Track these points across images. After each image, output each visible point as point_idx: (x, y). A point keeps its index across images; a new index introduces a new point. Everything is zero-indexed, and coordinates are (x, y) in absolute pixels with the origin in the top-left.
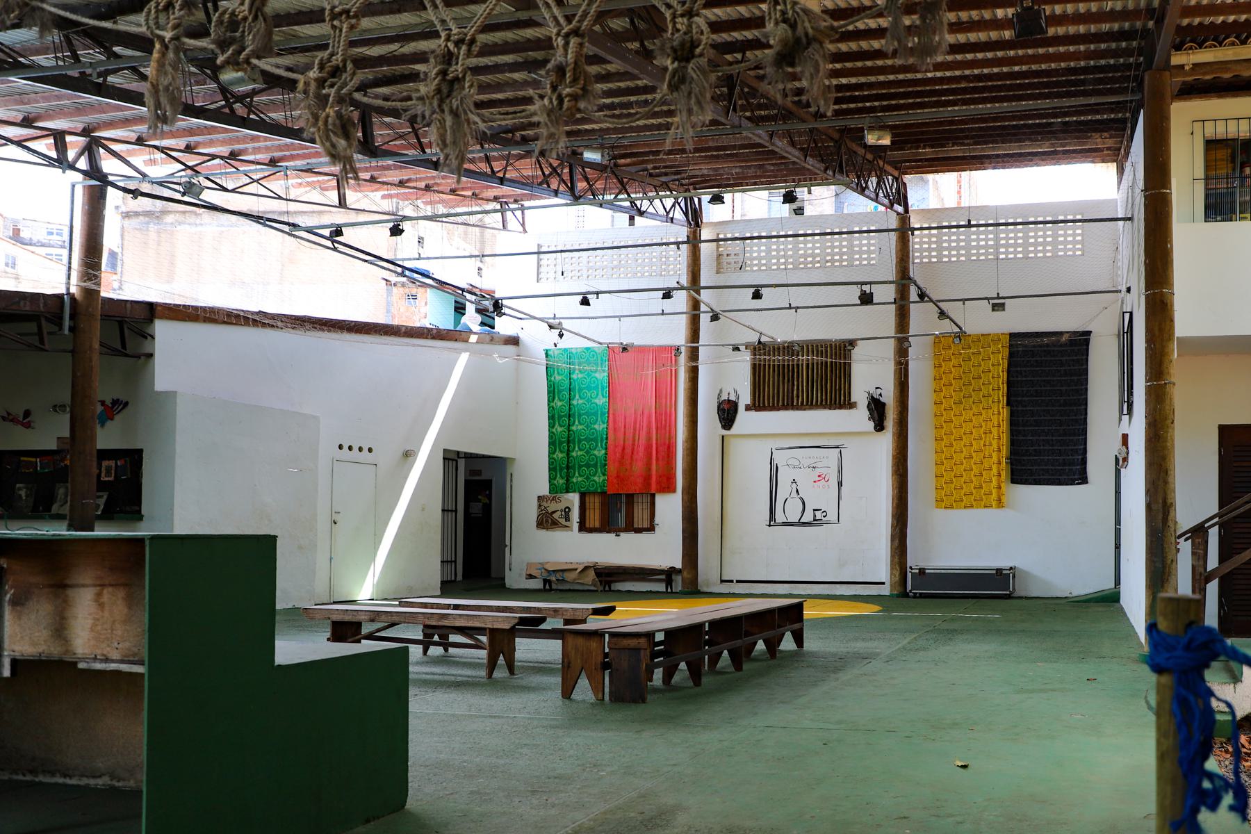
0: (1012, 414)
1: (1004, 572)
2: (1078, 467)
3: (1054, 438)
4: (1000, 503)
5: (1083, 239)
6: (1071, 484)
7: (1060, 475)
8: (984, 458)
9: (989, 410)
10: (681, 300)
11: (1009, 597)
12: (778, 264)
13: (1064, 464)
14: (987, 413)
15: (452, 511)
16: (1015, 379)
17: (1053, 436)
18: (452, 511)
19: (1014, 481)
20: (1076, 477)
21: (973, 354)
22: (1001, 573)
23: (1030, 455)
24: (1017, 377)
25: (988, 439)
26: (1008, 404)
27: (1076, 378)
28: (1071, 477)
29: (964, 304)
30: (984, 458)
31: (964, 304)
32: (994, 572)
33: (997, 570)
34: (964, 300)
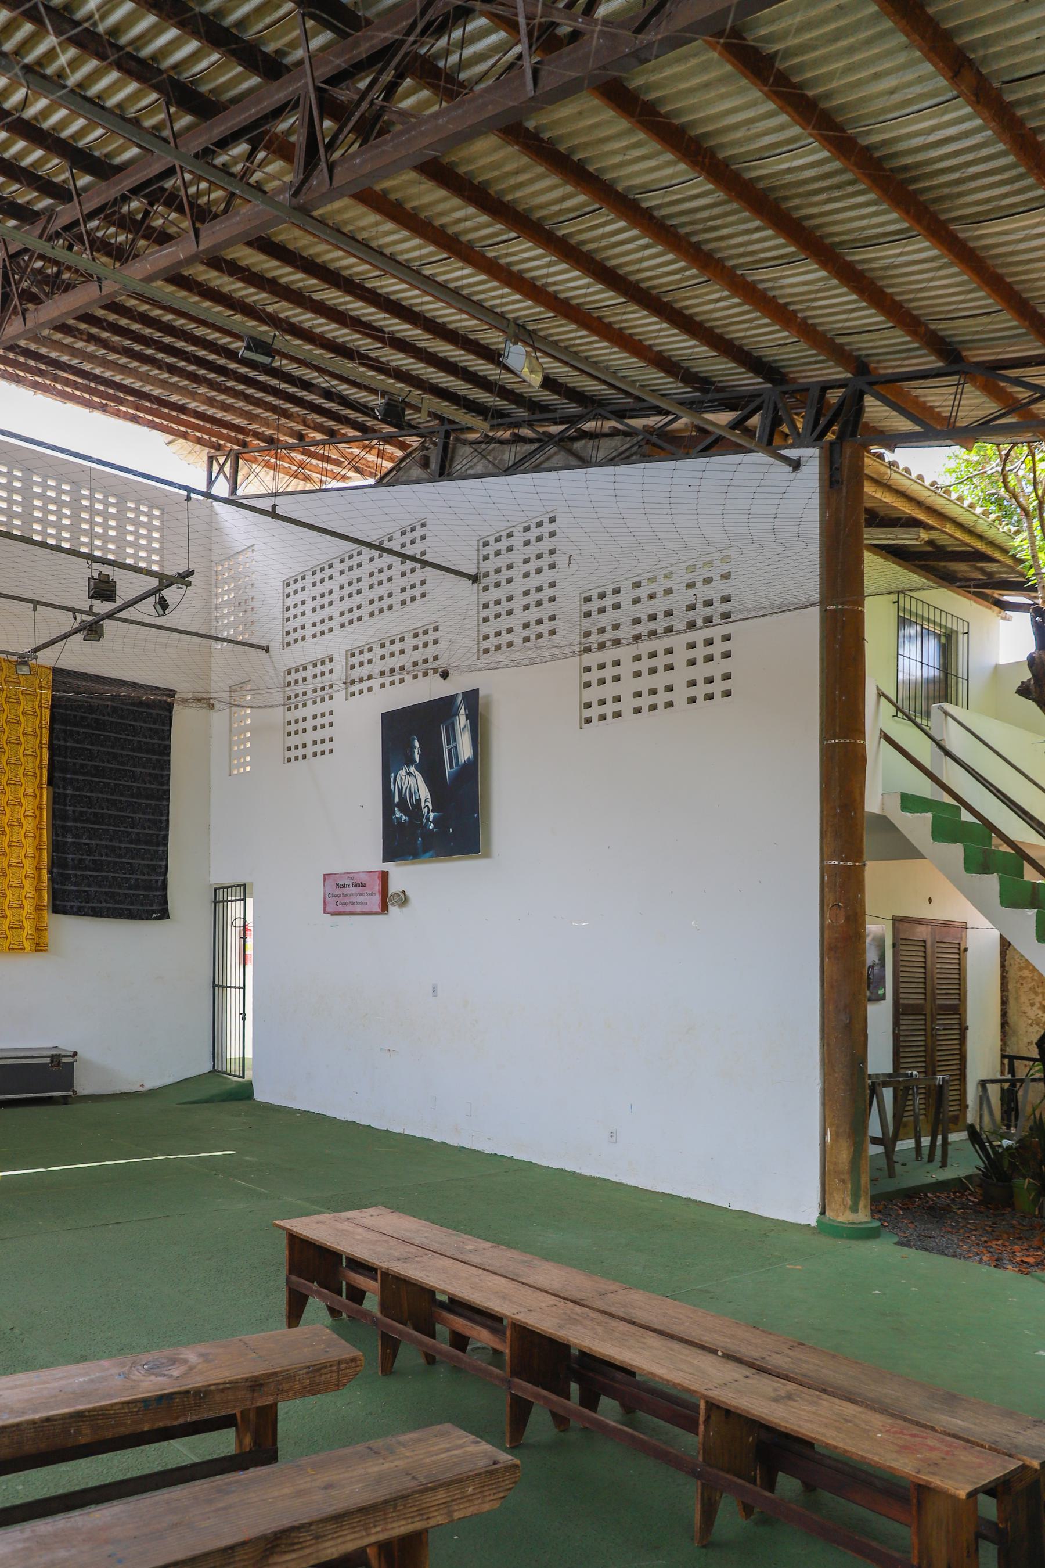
0: (57, 800)
1: (64, 1060)
2: (158, 893)
3: (123, 845)
4: (40, 947)
5: (162, 548)
6: (147, 919)
7: (132, 904)
8: (9, 866)
9: (18, 788)
10: (900, 715)
11: (65, 1100)
12: (107, 505)
13: (137, 887)
14: (14, 792)
15: (239, 988)
16: (62, 743)
17: (120, 842)
18: (239, 988)
19: (56, 909)
20: (154, 908)
21: (23, 693)
22: (59, 1062)
23: (85, 869)
24: (65, 740)
25: (15, 835)
26: (50, 783)
27: (155, 757)
28: (146, 908)
29: (35, 610)
30: (9, 866)
31: (35, 610)
32: (48, 1060)
33: (52, 1057)
34: (36, 603)
